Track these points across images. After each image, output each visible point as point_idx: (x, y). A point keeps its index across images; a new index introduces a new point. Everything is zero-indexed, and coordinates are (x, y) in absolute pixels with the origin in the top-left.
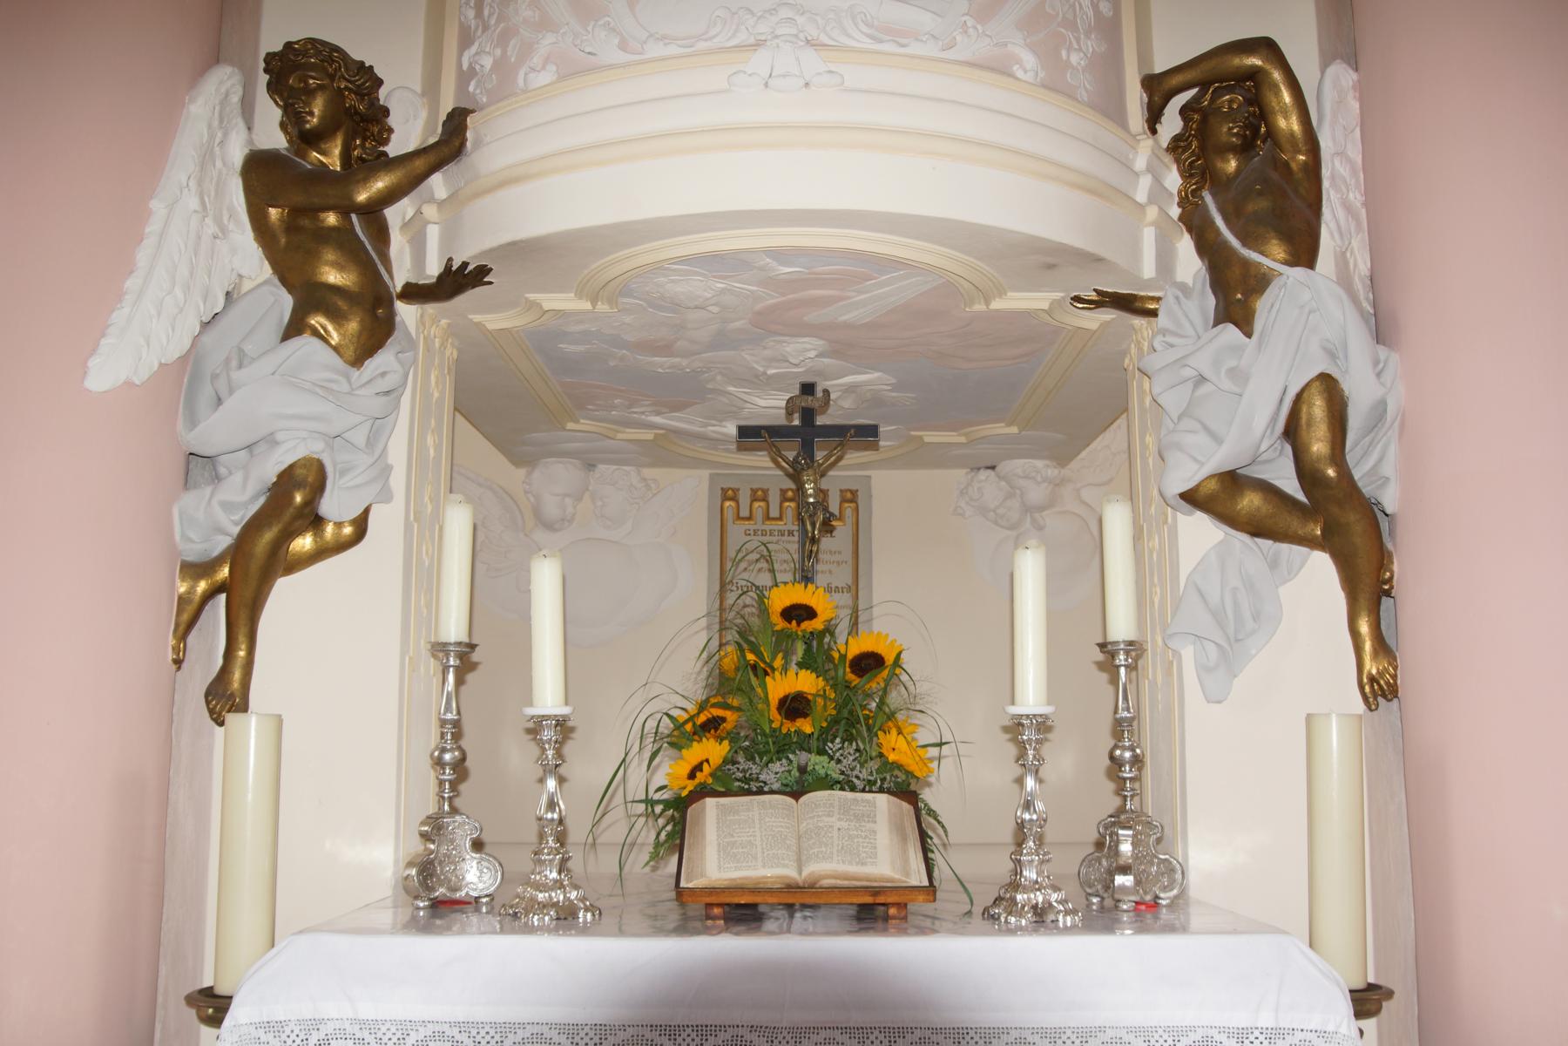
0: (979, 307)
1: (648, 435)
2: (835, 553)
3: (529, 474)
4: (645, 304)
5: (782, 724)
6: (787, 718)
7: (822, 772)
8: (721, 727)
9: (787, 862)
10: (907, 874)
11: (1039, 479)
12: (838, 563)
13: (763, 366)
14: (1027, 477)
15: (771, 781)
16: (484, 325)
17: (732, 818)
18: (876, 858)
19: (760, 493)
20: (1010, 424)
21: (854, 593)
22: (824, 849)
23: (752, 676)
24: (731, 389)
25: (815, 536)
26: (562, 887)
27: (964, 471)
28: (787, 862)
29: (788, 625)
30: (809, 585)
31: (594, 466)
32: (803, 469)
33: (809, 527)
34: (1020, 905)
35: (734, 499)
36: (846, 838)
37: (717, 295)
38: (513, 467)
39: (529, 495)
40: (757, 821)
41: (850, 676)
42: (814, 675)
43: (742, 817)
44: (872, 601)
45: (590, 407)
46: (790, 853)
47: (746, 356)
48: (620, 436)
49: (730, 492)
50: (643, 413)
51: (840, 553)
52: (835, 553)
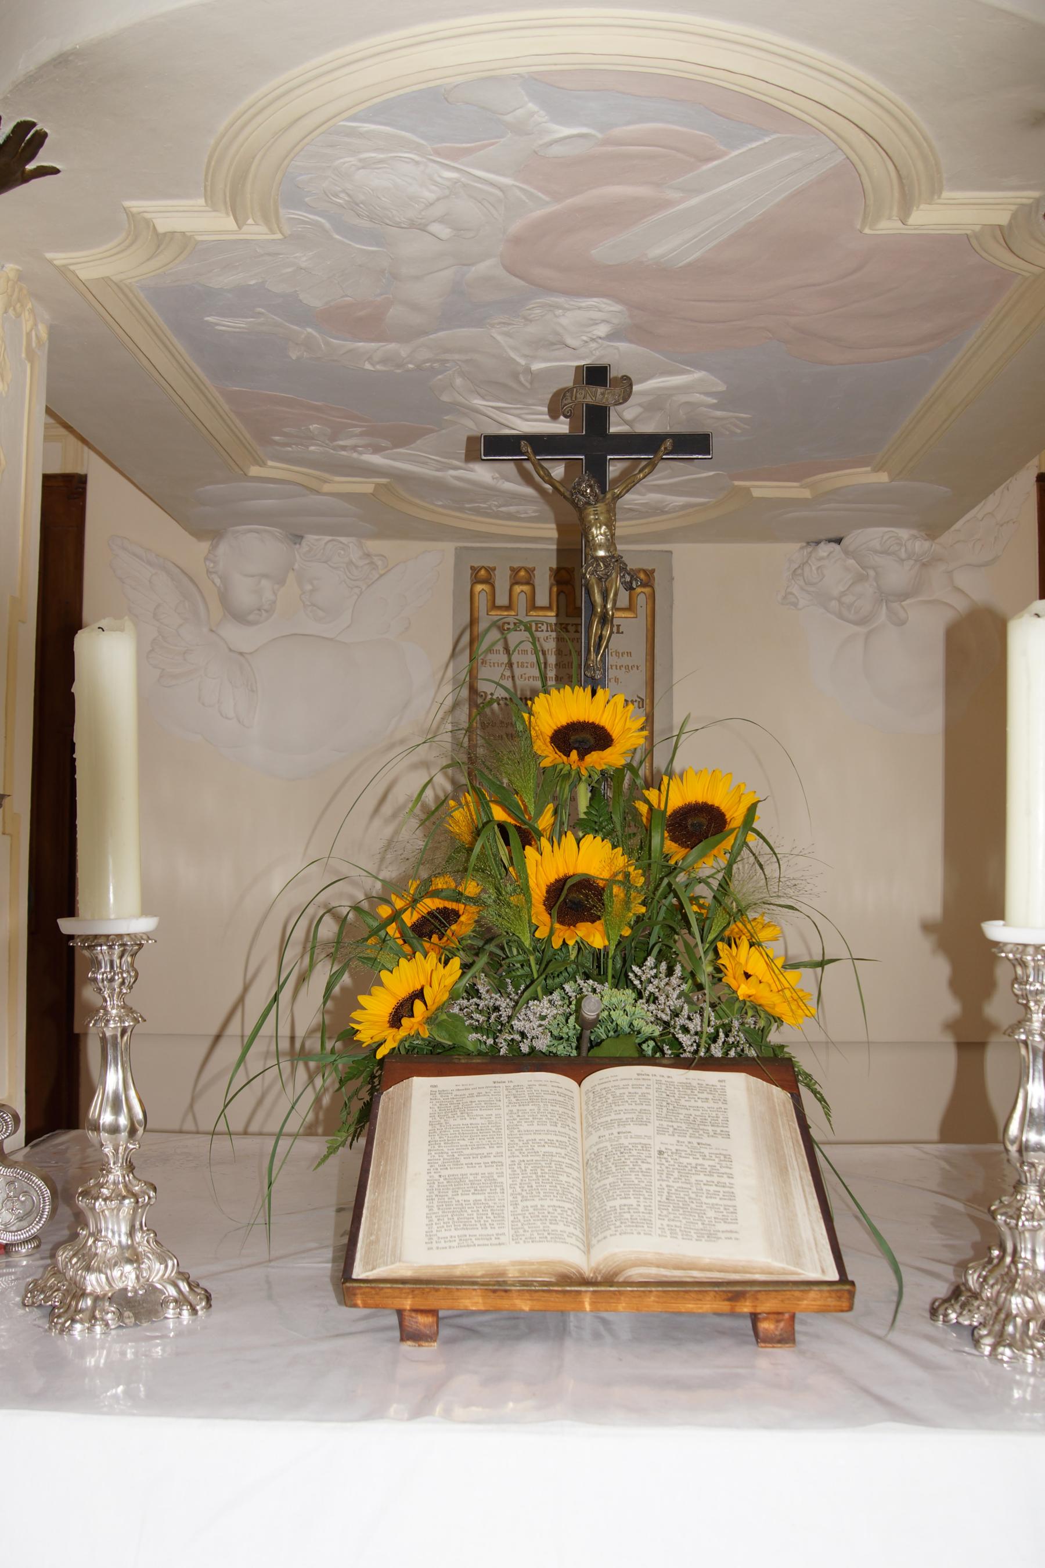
0: (888, 226)
1: (365, 486)
2: (623, 654)
3: (214, 547)
4: (327, 225)
5: (552, 932)
6: (561, 923)
7: (623, 1021)
8: (449, 933)
9: (560, 1227)
10: (797, 1256)
11: (903, 555)
12: (627, 667)
13: (525, 356)
14: (886, 552)
15: (534, 1033)
16: (73, 272)
17: (459, 1121)
18: (735, 1221)
19: (522, 573)
20: (877, 469)
21: (648, 709)
22: (633, 1201)
23: (500, 842)
24: (478, 402)
25: (607, 612)
26: (135, 1259)
27: (799, 545)
28: (560, 1227)
29: (565, 758)
30: (600, 692)
31: (302, 537)
32: (588, 503)
33: (598, 598)
34: (1019, 1320)
35: (488, 581)
36: (676, 1174)
37: (446, 197)
38: (193, 539)
39: (214, 576)
40: (505, 1132)
41: (670, 846)
42: (608, 844)
43: (478, 1120)
44: (672, 719)
45: (277, 438)
46: (567, 1205)
47: (499, 338)
48: (327, 488)
49: (483, 572)
50: (354, 448)
51: (629, 654)
52: (623, 654)
